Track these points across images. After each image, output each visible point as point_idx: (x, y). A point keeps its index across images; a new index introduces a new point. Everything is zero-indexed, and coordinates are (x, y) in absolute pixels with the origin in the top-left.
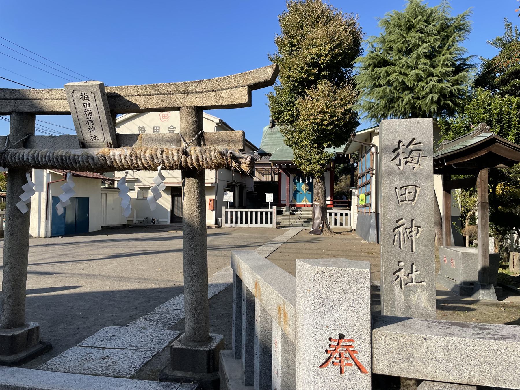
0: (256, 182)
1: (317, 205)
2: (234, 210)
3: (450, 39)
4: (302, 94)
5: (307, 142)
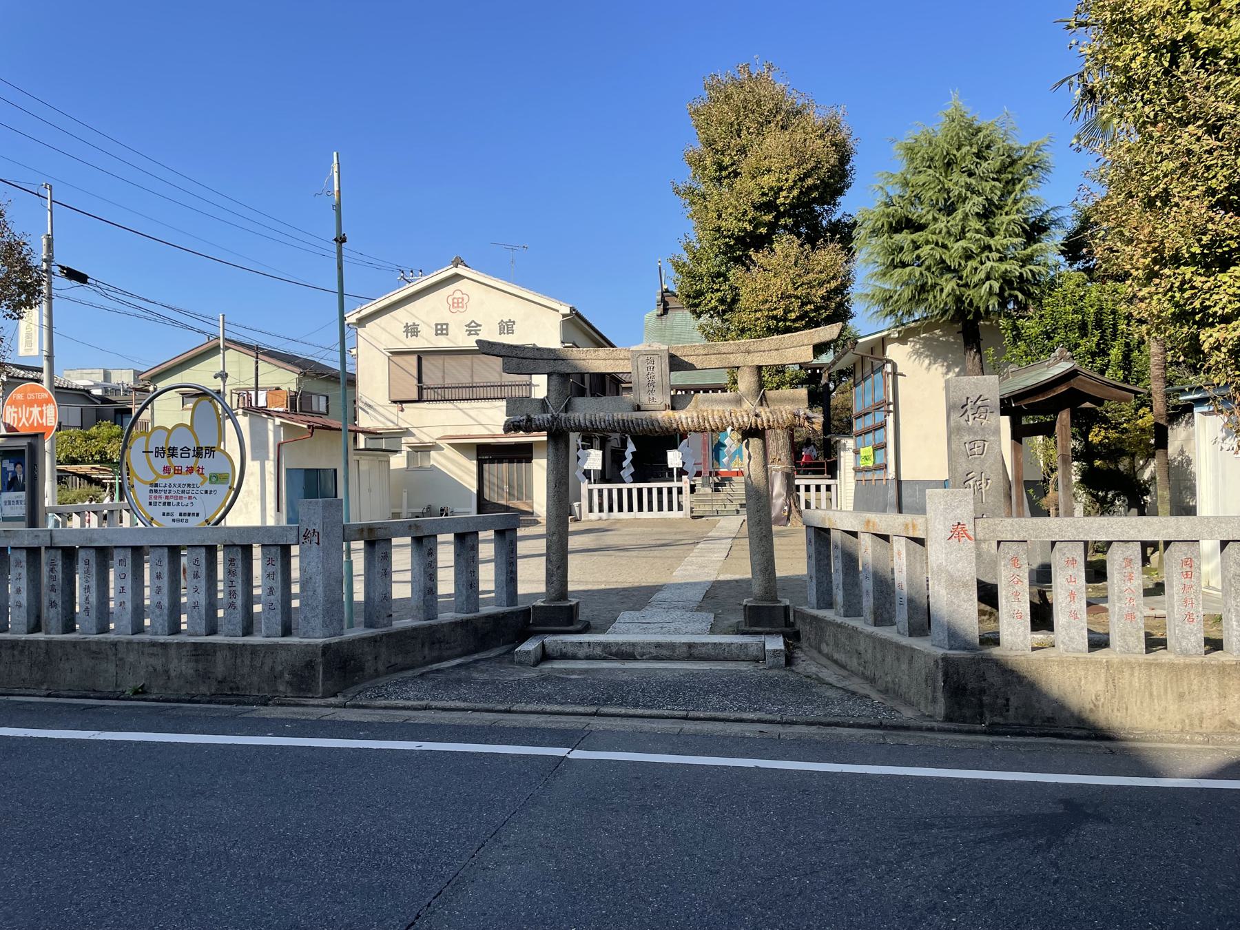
1: (777, 471)
3: (1018, 187)
4: (743, 261)
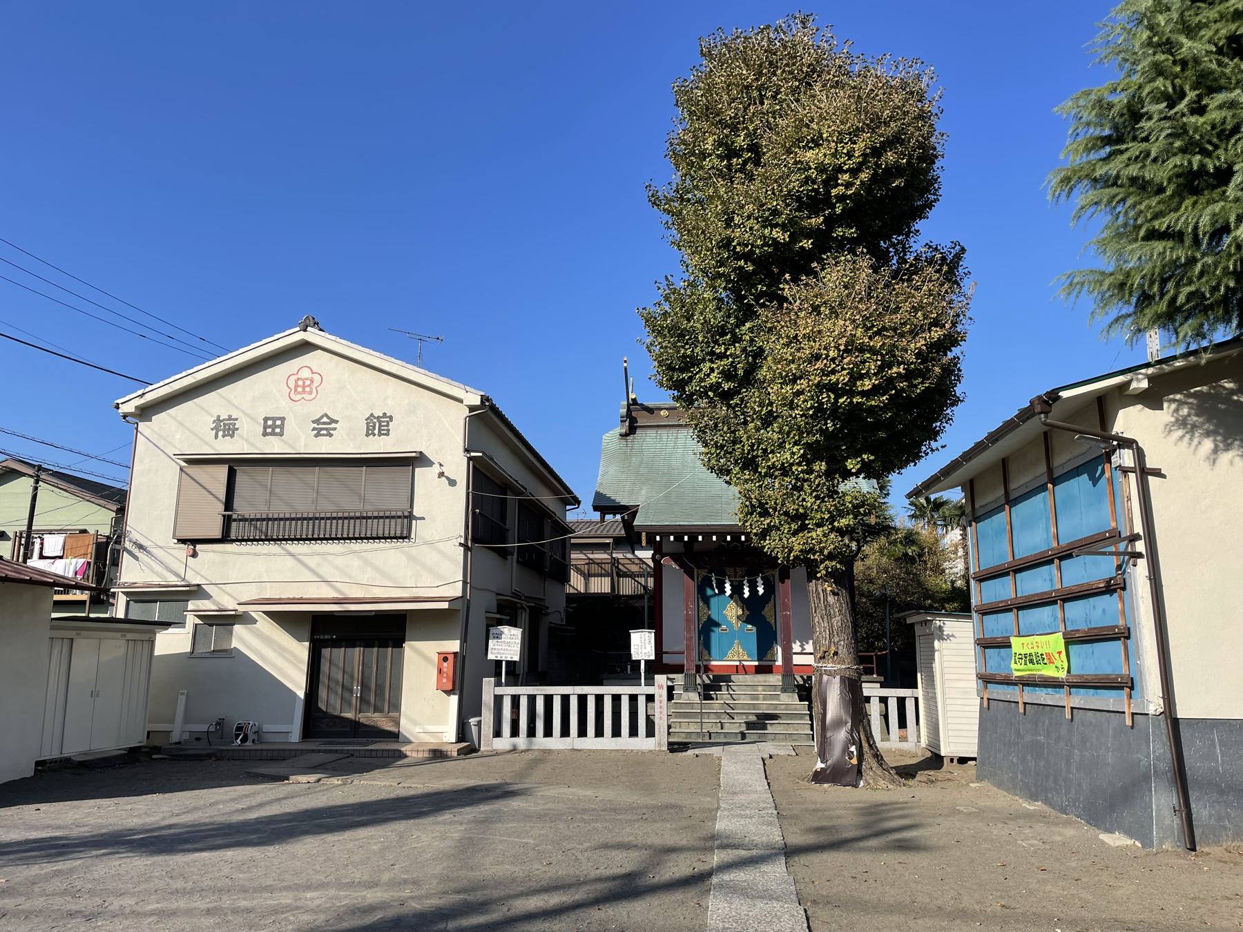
0: (572, 599)
1: (830, 674)
2: (523, 691)
5: (790, 454)
